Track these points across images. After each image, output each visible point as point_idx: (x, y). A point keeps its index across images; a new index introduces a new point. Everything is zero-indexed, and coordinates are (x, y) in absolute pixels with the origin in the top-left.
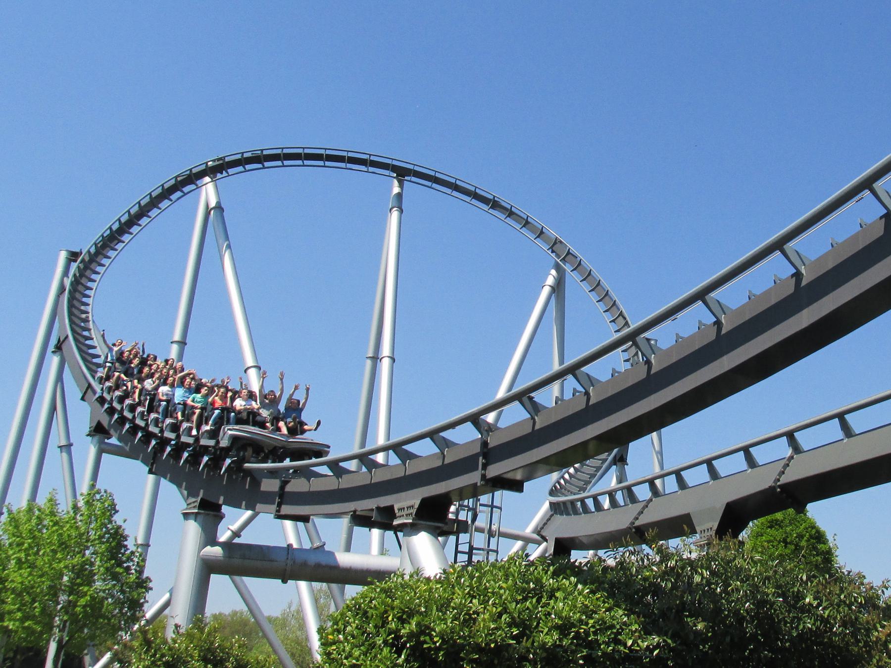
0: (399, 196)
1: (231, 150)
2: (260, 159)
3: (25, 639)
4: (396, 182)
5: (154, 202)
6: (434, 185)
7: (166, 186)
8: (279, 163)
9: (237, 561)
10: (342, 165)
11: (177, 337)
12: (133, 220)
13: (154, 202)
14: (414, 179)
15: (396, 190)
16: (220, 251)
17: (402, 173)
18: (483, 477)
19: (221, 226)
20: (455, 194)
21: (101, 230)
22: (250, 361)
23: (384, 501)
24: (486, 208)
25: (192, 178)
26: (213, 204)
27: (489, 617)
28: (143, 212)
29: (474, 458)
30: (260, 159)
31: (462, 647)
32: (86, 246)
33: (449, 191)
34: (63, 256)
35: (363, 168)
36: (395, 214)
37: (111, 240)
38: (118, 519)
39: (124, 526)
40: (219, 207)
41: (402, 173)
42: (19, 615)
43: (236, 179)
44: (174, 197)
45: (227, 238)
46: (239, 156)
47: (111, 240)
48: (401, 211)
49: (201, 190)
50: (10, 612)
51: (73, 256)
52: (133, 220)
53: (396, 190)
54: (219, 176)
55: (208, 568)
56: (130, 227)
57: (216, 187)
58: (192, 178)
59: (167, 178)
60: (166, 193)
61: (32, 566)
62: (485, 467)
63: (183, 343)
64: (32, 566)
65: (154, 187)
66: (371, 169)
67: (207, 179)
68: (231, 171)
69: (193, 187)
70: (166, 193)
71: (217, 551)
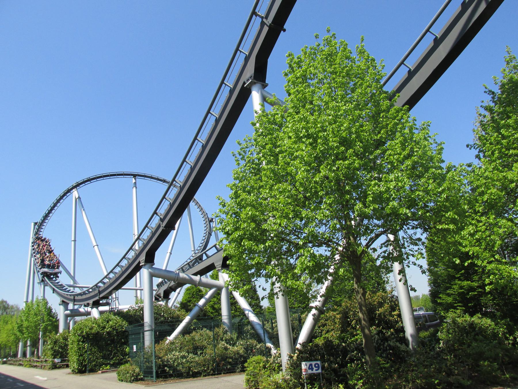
0: (135, 183)
1: (80, 179)
2: (89, 180)
3: (89, 331)
4: (133, 179)
5: (58, 201)
6: (145, 178)
7: (61, 195)
8: (96, 180)
9: (73, 314)
10: (116, 177)
11: (73, 239)
12: (52, 208)
13: (58, 201)
14: (139, 177)
15: (134, 181)
16: (81, 211)
17: (135, 176)
18: (99, 297)
19: (81, 204)
20: (152, 180)
21: (43, 214)
22: (95, 244)
23: (88, 302)
24: (162, 183)
25: (69, 191)
26: (77, 197)
27: (176, 314)
28: (55, 205)
29: (97, 294)
30: (89, 180)
31: (89, 334)
32: (39, 220)
33: (150, 179)
34: (33, 224)
35: (123, 176)
36: (134, 189)
37: (46, 217)
38: (49, 305)
39: (51, 306)
40: (79, 198)
41: (135, 176)
42: (27, 333)
43: (83, 188)
44: (64, 198)
45: (83, 207)
46: (83, 181)
47: (46, 217)
48: (136, 188)
49: (73, 195)
50: (25, 333)
51: (36, 223)
52: (52, 208)
53: (134, 181)
54: (78, 188)
55: (67, 316)
56: (52, 211)
57: (77, 191)
58: (69, 191)
59: (61, 193)
60: (62, 198)
61: (28, 321)
62: (99, 295)
63: (75, 241)
64: (28, 321)
65: (57, 196)
66: (125, 176)
67: (74, 190)
68: (81, 186)
69: (70, 193)
70: (62, 198)
71: (68, 312)
